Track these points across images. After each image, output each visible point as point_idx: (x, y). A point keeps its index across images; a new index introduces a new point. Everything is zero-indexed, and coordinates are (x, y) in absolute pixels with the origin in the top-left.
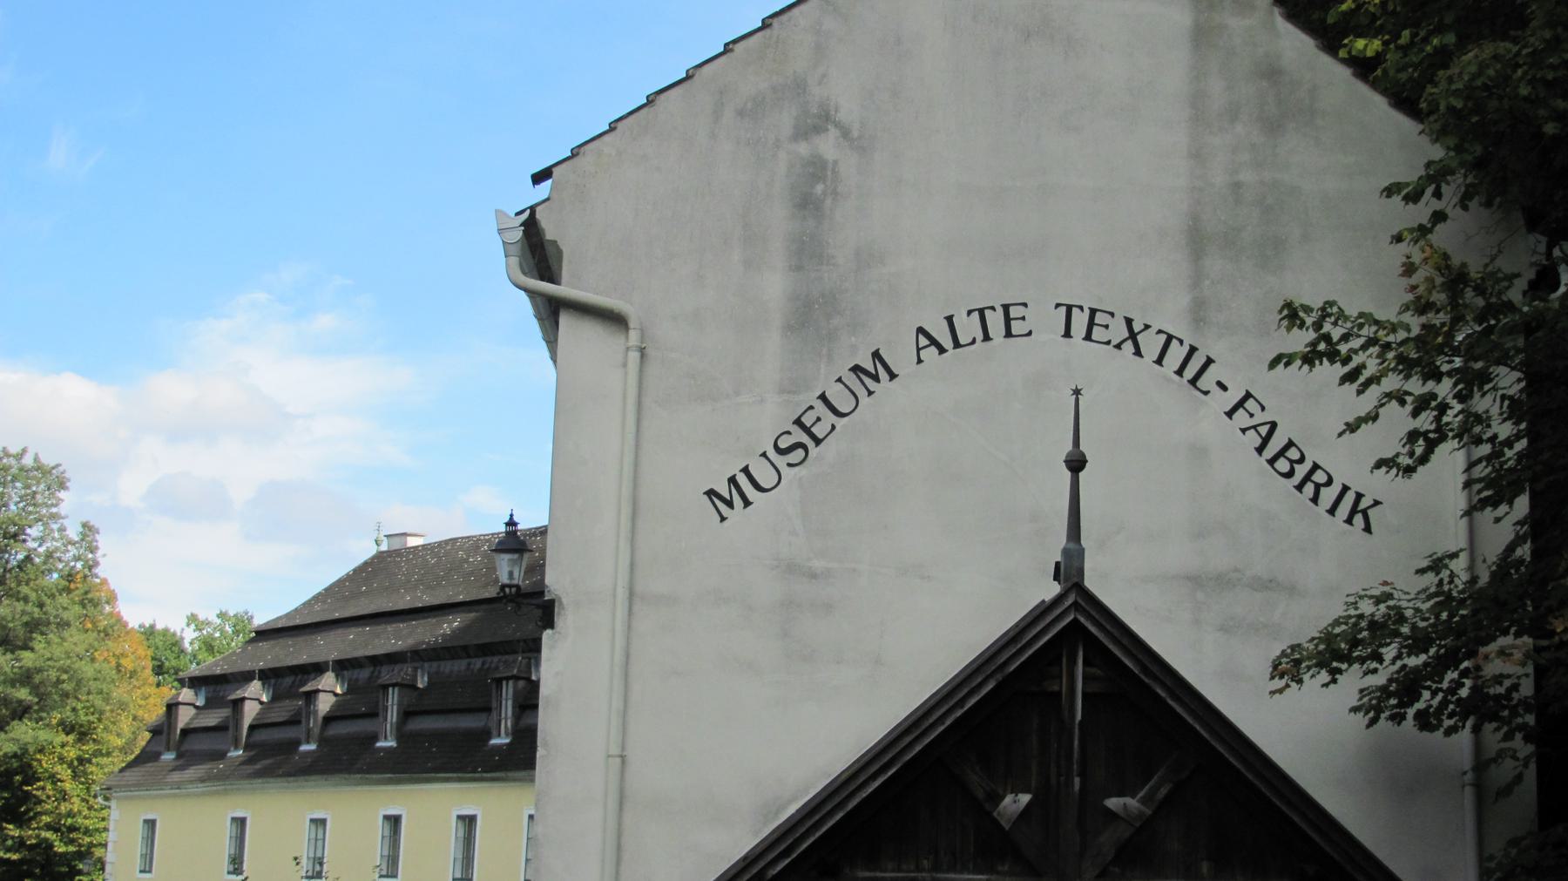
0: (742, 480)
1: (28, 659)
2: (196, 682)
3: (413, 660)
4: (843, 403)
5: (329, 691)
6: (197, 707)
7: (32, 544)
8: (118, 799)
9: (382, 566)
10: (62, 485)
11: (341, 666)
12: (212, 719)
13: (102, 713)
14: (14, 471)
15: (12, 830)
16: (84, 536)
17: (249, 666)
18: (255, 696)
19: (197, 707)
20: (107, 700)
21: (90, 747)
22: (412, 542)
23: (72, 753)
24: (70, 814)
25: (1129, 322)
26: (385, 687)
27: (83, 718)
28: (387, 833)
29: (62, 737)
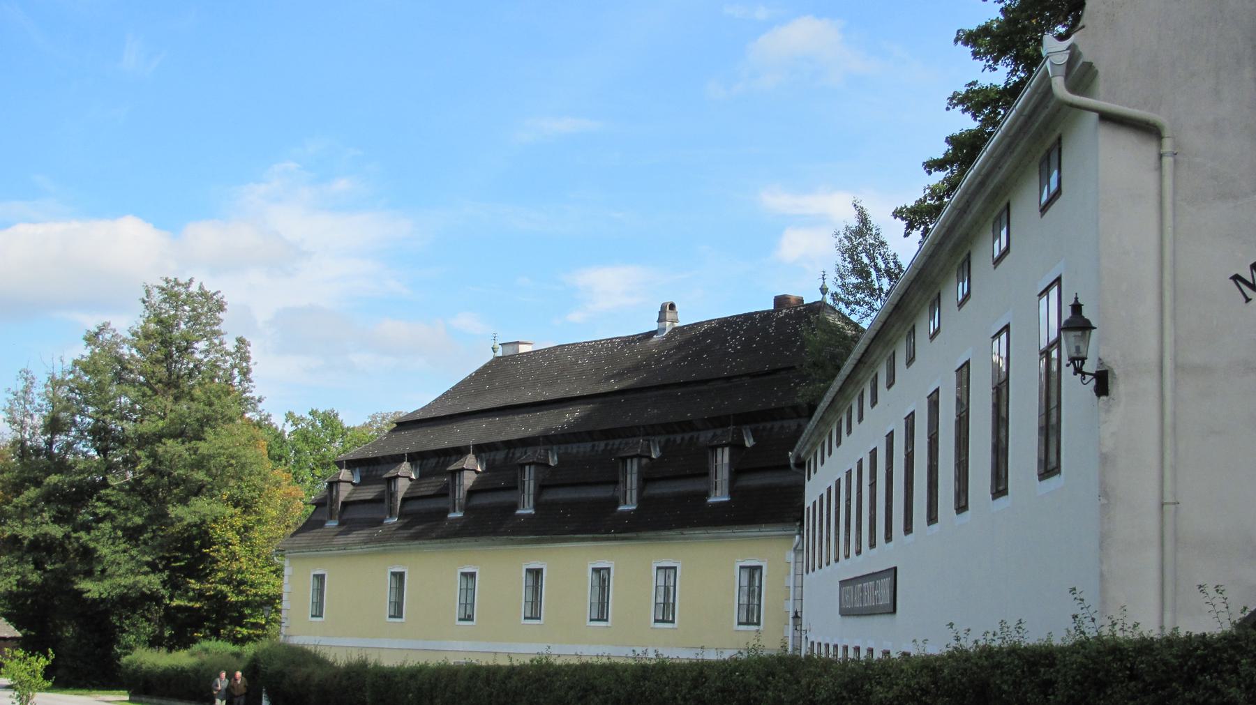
1: (203, 447)
2: (351, 464)
3: (544, 444)
5: (471, 469)
6: (353, 484)
7: (198, 356)
8: (290, 558)
9: (503, 368)
10: (221, 308)
11: (480, 450)
12: (369, 493)
13: (261, 490)
14: (183, 296)
15: (194, 584)
16: (238, 349)
17: (397, 451)
18: (405, 477)
19: (353, 484)
20: (265, 479)
21: (253, 518)
22: (523, 349)
23: (238, 522)
24: (240, 571)
26: (522, 466)
27: (247, 495)
28: (394, 585)
29: (231, 510)
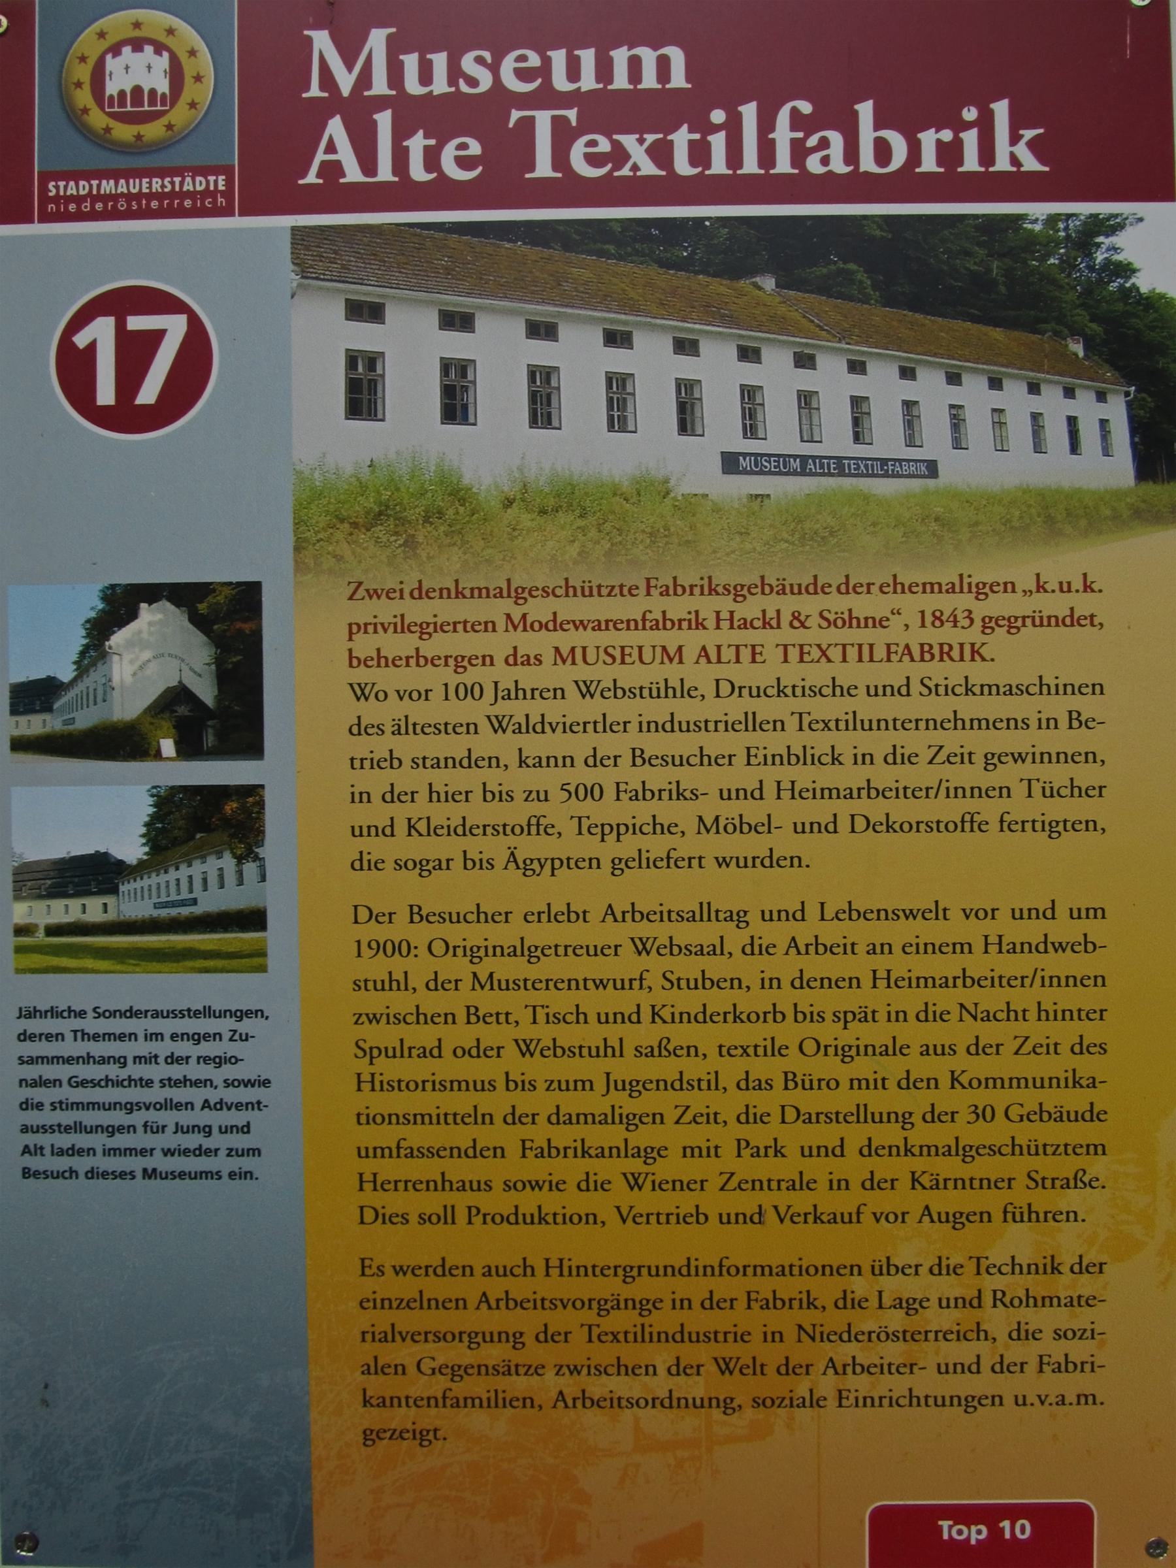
0: (579, 652)
4: (647, 657)
25: (819, 646)
